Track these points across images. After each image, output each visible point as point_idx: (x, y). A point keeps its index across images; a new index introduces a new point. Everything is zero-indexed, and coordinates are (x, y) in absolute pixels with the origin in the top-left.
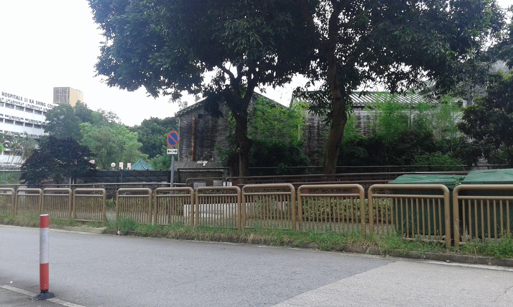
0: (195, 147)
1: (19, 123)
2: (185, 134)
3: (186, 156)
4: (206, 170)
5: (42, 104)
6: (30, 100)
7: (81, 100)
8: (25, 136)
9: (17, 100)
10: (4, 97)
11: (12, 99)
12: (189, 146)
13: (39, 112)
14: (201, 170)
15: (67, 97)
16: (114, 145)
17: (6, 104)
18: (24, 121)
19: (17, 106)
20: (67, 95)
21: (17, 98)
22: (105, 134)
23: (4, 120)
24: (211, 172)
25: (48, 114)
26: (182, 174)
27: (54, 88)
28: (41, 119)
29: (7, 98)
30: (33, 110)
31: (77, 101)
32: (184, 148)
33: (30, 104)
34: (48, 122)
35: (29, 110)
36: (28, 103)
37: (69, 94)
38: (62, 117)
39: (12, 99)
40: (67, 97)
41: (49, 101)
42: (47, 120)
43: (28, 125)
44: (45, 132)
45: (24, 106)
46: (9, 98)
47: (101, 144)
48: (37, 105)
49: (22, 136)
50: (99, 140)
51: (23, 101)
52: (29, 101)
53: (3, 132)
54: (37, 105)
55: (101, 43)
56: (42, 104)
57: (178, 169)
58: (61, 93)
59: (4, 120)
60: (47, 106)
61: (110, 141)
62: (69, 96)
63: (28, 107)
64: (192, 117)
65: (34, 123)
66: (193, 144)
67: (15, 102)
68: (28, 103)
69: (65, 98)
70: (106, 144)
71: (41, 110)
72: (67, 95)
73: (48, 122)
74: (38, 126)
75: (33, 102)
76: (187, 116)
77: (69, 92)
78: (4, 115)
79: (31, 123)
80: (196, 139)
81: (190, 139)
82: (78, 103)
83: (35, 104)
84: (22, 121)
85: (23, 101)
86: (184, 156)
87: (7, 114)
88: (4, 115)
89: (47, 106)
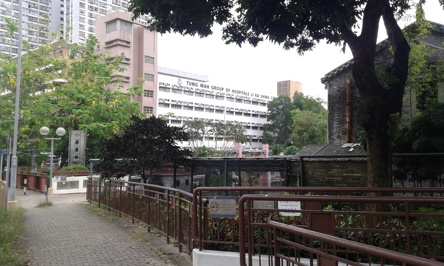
0: (351, 123)
1: (247, 115)
2: (337, 105)
3: (339, 137)
4: (347, 159)
5: (266, 97)
6: (256, 95)
7: (297, 90)
8: (235, 124)
9: (205, 89)
10: (234, 94)
11: (240, 95)
12: (342, 122)
13: (264, 104)
14: (339, 159)
15: (288, 89)
16: (317, 129)
17: (216, 96)
18: (251, 112)
19: (261, 103)
20: (288, 87)
21: (245, 94)
22: (307, 119)
23: (234, 113)
24: (356, 161)
25: (271, 106)
26: (307, 165)
27: (278, 83)
28: (264, 109)
29: (237, 94)
30: (258, 103)
31: (295, 92)
32: (335, 126)
33: (256, 98)
34: (270, 112)
35: (255, 103)
36: (254, 97)
37: (289, 86)
38: (281, 107)
39: (240, 95)
40: (288, 89)
41: (273, 93)
42: (269, 110)
43: (254, 115)
44: (268, 121)
45: (251, 100)
46: (238, 95)
47: (303, 129)
48: (262, 99)
49: (233, 124)
50: (301, 125)
51: (250, 96)
52: (254, 95)
53: (193, 118)
54: (262, 99)
55: (344, 49)
56: (266, 97)
57: (302, 158)
58: (283, 86)
59: (234, 113)
60: (270, 98)
61: (311, 125)
62: (289, 88)
63: (254, 100)
64: (345, 80)
65: (259, 114)
66: (348, 119)
67: (204, 91)
68: (254, 97)
69: (287, 91)
70: (308, 128)
71: (265, 102)
72: (288, 87)
73: (270, 112)
74: (263, 116)
75: (258, 96)
76: (338, 79)
77: (289, 84)
78: (234, 109)
79: (257, 113)
80: (352, 111)
81: (344, 112)
82: (296, 93)
83: (260, 98)
84: (249, 112)
85: (250, 96)
86: (335, 137)
87: (217, 105)
88: (234, 109)
89: (270, 98)
